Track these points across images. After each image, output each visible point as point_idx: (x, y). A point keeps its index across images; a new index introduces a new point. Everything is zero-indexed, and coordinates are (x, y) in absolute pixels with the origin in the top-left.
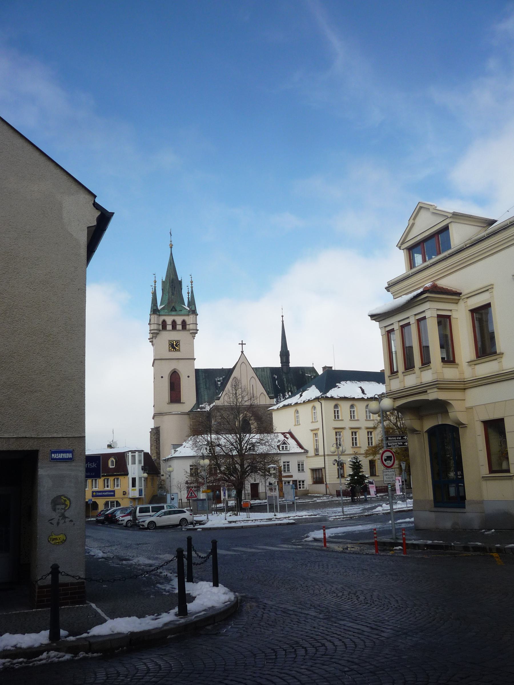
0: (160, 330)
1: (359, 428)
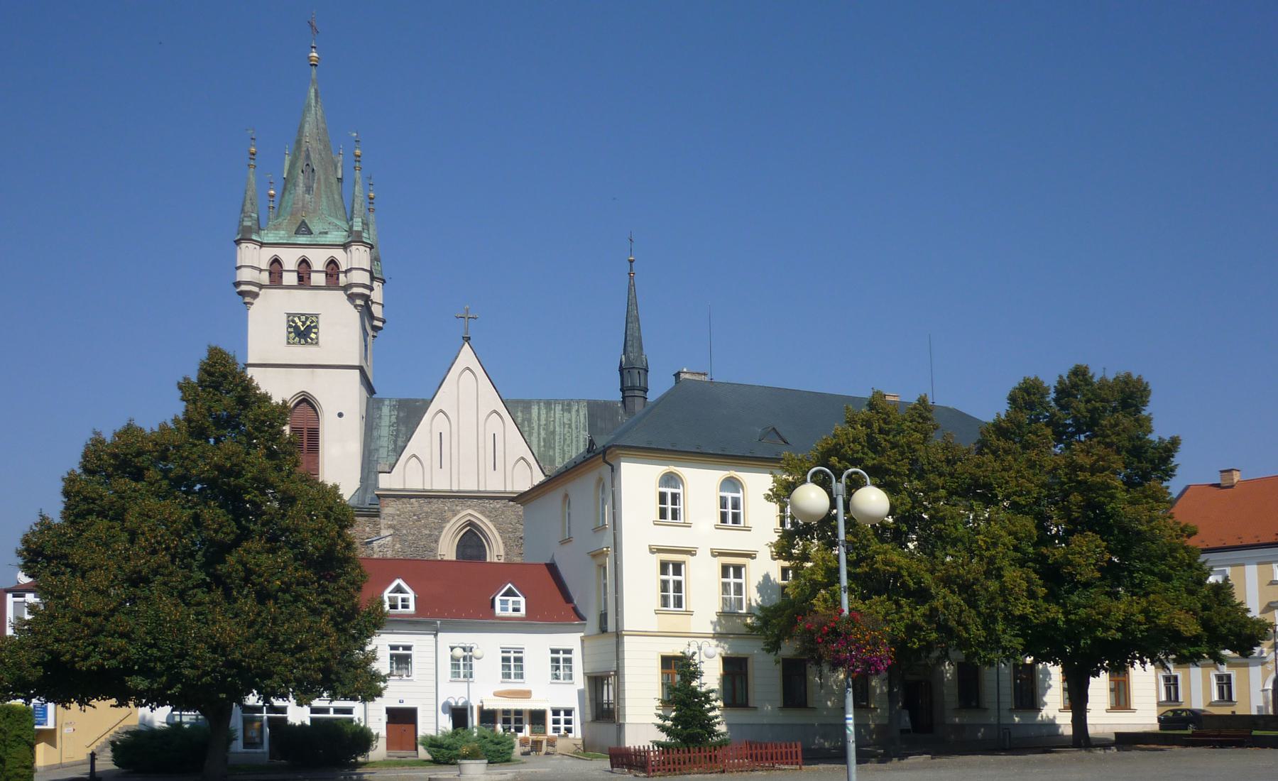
0: (261, 286)
1: (690, 552)
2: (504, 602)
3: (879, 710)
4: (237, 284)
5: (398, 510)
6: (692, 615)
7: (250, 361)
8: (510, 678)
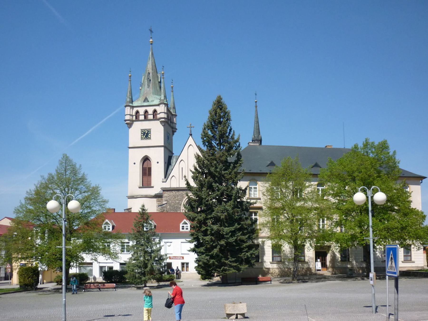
5: (169, 195)
7: (130, 146)
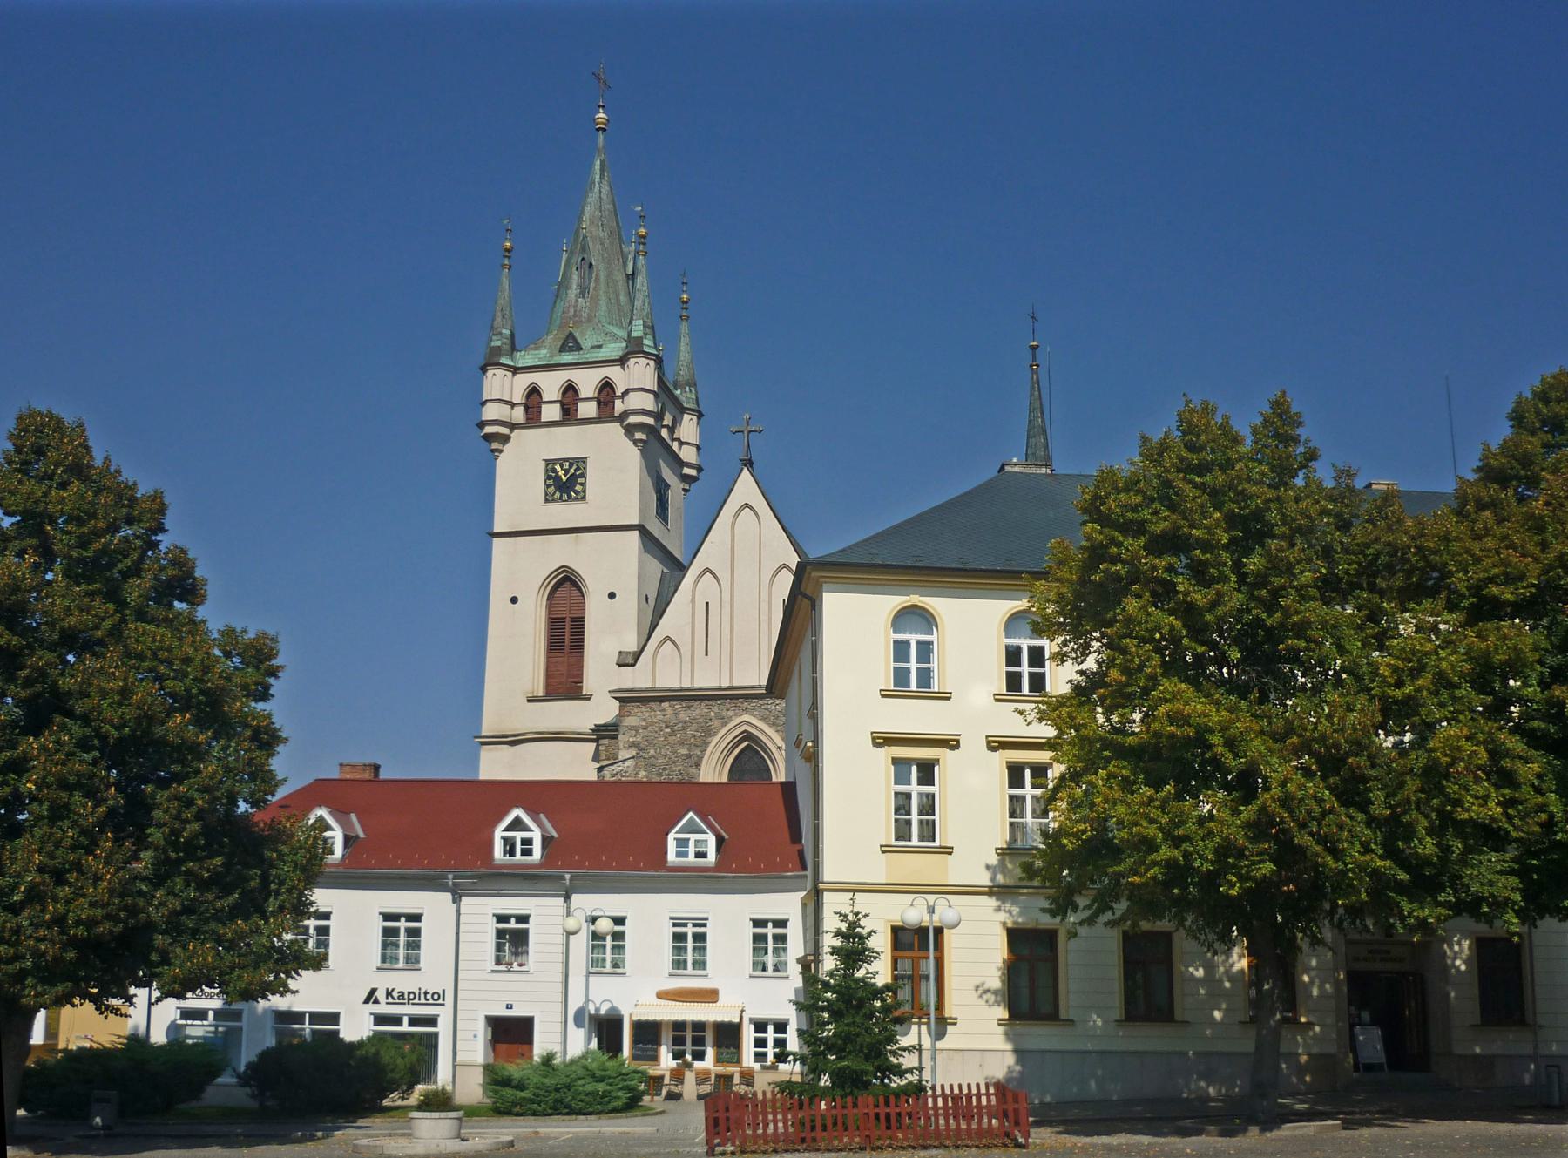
0: (513, 426)
1: (950, 743)
2: (683, 843)
3: (1317, 1029)
4: (482, 425)
5: (645, 720)
6: (950, 853)
7: (497, 529)
8: (685, 968)
